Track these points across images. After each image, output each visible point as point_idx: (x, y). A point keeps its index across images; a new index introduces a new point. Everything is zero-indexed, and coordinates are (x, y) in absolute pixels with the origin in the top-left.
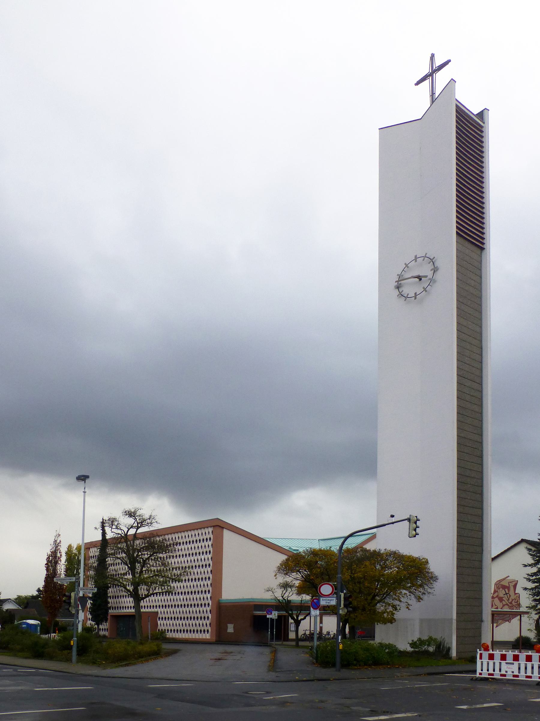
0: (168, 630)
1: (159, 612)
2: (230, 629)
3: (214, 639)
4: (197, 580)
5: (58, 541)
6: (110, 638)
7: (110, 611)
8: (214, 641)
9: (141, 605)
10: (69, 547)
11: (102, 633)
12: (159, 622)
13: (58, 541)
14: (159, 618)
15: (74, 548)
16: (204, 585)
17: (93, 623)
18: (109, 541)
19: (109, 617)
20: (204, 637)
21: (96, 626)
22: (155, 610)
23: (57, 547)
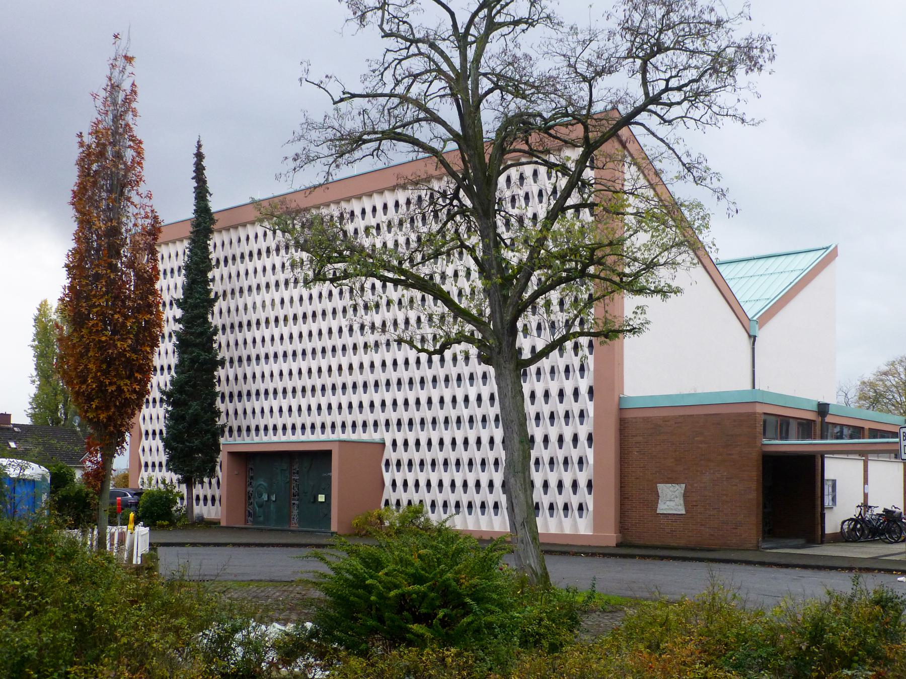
0: (433, 505)
1: (389, 444)
2: (671, 500)
3: (610, 537)
4: (262, 396)
5: (126, 86)
6: (228, 528)
7: (222, 440)
8: (613, 543)
9: (526, 389)
10: (41, 305)
11: (199, 510)
12: (387, 478)
13: (126, 86)
14: (387, 463)
15: (53, 310)
16: (236, 413)
17: (175, 477)
18: (216, 217)
19: (222, 458)
20: (568, 530)
21: (183, 489)
22: (371, 436)
23: (117, 118)
